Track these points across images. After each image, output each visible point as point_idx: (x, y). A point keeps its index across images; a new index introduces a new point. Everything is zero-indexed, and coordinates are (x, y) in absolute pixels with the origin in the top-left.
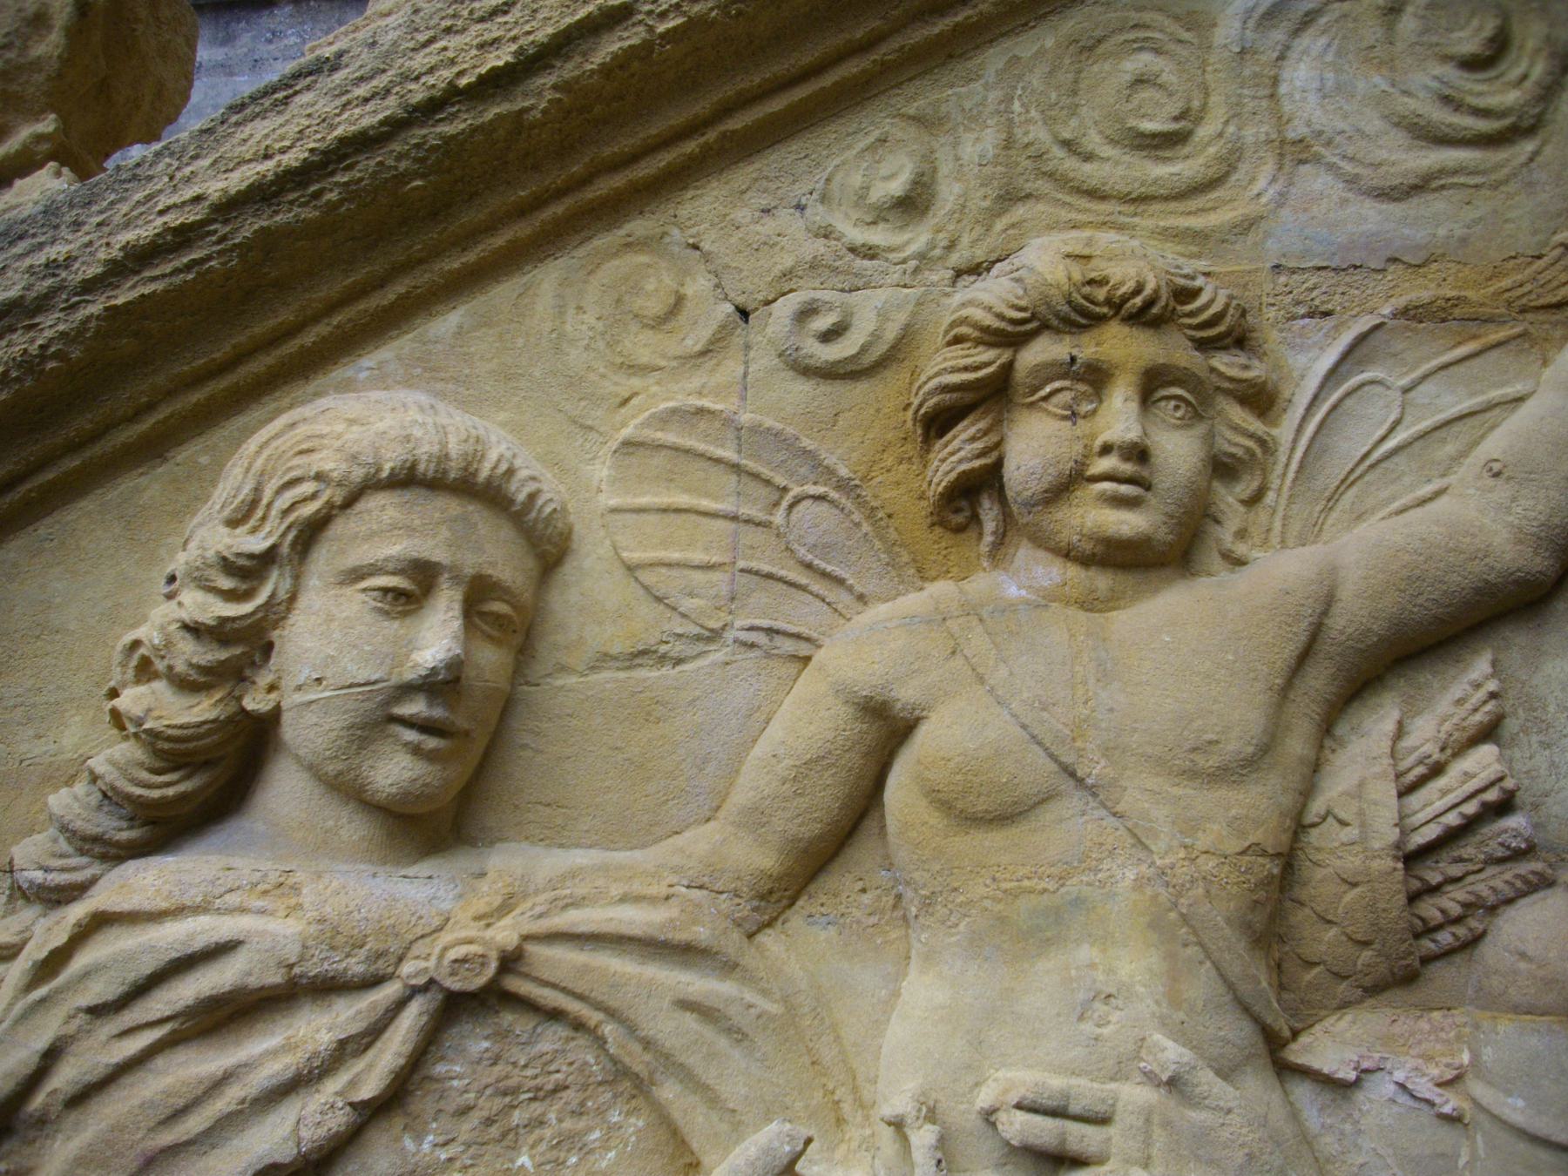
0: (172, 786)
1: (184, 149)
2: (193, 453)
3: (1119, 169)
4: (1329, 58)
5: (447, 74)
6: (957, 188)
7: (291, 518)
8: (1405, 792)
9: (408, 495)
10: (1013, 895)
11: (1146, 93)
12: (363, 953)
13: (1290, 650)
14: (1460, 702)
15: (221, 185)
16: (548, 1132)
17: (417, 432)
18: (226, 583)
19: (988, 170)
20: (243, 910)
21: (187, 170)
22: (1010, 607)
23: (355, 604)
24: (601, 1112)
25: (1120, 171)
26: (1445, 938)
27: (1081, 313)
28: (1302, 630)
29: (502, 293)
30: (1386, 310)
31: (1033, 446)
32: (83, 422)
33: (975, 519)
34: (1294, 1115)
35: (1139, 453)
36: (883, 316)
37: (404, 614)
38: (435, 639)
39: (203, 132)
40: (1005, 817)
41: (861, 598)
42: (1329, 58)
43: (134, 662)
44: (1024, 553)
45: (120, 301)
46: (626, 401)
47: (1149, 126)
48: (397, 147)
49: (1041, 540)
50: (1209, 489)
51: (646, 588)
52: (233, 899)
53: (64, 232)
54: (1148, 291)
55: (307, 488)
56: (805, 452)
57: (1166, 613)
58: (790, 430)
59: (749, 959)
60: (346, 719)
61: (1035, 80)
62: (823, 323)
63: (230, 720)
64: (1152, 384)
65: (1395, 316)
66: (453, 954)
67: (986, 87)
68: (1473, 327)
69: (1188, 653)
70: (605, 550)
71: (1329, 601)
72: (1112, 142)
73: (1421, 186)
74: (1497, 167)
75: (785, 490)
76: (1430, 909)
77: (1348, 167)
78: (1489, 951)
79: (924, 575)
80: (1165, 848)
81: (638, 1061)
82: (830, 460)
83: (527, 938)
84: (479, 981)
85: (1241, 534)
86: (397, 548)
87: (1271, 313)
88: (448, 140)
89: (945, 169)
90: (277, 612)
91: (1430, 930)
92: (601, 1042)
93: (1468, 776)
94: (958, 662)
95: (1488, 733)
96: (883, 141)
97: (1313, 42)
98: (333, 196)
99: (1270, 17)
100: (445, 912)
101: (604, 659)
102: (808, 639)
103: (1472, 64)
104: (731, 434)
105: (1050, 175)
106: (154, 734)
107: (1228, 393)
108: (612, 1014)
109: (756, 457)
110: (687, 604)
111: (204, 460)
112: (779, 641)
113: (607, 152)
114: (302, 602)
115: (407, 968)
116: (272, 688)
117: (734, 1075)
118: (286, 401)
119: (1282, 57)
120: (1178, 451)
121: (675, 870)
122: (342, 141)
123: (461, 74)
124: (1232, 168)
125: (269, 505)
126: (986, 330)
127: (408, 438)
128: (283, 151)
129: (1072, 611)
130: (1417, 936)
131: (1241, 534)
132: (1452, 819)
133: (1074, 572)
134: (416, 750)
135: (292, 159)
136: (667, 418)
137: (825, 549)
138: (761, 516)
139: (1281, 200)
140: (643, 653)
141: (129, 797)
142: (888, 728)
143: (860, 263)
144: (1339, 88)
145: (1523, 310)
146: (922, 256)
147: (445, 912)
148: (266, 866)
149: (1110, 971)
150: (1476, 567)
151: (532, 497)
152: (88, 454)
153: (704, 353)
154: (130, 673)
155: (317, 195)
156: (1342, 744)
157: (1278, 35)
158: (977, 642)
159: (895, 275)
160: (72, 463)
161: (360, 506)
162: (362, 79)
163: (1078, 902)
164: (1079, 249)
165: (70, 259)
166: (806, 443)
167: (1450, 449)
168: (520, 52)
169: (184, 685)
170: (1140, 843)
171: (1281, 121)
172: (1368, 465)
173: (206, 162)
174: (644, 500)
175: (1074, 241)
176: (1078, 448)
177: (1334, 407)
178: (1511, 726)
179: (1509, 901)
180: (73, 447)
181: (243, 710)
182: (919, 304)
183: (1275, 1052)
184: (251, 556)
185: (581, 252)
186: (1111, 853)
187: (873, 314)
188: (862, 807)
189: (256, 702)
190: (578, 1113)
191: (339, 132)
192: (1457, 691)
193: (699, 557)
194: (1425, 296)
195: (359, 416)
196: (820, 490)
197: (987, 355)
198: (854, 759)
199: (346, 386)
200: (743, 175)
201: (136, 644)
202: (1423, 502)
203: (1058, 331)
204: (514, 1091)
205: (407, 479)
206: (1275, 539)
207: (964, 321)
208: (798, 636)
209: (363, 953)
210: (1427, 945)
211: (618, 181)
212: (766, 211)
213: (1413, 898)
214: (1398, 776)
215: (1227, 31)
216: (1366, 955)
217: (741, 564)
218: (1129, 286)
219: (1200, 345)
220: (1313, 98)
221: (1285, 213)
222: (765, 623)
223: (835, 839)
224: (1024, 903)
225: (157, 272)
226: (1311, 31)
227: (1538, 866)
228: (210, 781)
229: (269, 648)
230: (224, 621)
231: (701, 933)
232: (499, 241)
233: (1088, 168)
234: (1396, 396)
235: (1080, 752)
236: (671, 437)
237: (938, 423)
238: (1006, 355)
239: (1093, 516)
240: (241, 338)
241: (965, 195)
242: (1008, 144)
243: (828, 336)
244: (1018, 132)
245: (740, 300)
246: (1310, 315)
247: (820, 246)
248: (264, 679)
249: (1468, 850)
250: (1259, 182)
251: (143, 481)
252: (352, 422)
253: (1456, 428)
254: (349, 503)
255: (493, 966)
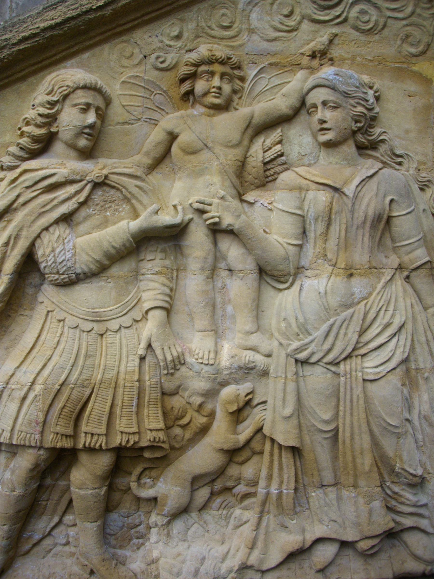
0: (35, 146)
1: (34, 16)
2: (32, 79)
3: (218, 32)
4: (260, 12)
5: (90, 6)
6: (187, 34)
7: (62, 94)
8: (264, 152)
9: (85, 90)
10: (196, 166)
11: (224, 17)
12: (79, 175)
13: (245, 126)
14: (275, 137)
15: (43, 25)
16: (112, 209)
17: (86, 78)
18: (48, 106)
19: (193, 31)
20: (55, 168)
21: (35, 21)
22: (195, 116)
23: (75, 111)
24: (122, 205)
25: (218, 33)
26: (270, 178)
27: (210, 62)
28: (247, 122)
29: (97, 50)
30: (266, 63)
31: (200, 86)
32: (10, 72)
33: (189, 99)
34: (243, 208)
35: (220, 88)
36: (172, 59)
37: (84, 113)
38: (91, 118)
39: (38, 13)
40: (194, 152)
41: (167, 113)
42: (260, 12)
43: (25, 122)
44: (198, 106)
45: (21, 48)
46: (122, 73)
47: (225, 24)
48: (79, 20)
49: (201, 104)
50: (232, 96)
51: (127, 110)
52: (53, 166)
53: (8, 32)
54: (223, 58)
55: (65, 88)
56: (158, 85)
57: (223, 118)
58: (155, 81)
59: (147, 179)
60: (75, 132)
61: (203, 13)
62: (161, 60)
63: (48, 133)
64: (223, 75)
65: (268, 64)
66: (96, 175)
67: (194, 14)
68: (282, 68)
69: (227, 125)
70: (118, 102)
71: (252, 117)
72: (217, 27)
73: (275, 39)
74: (289, 37)
75: (153, 92)
76: (268, 173)
77: (261, 35)
78: (278, 181)
79: (179, 109)
80: (222, 159)
81: (129, 196)
82: (162, 87)
83: (109, 173)
84: (101, 180)
85: (237, 104)
86: (83, 100)
87: (245, 63)
88: (90, 19)
89: (185, 30)
90: (58, 112)
91: (268, 177)
92: (122, 192)
93: (275, 149)
94: (186, 125)
95: (280, 142)
96: (173, 24)
97: (257, 9)
98: (66, 29)
99: (249, 3)
100: (94, 169)
101: (118, 123)
102: (157, 121)
103: (286, 16)
104: (143, 81)
105: (205, 33)
106: (33, 136)
107: (236, 78)
108: (124, 187)
109: (148, 85)
110: (134, 113)
111: (35, 81)
112: (152, 121)
113: (120, 23)
114: (64, 110)
115: (88, 178)
116: (57, 127)
117: (145, 199)
118: (52, 70)
119: (251, 12)
120: (227, 88)
121: (133, 163)
122: (68, 18)
123: (93, 6)
124: (240, 33)
125: (56, 91)
126: (192, 63)
127: (84, 79)
128: (56, 19)
129: (206, 117)
130: (266, 178)
131: (237, 104)
132: (272, 157)
133: (207, 110)
134: (87, 139)
135: (59, 20)
136: (131, 77)
137: (160, 103)
138: (149, 97)
139: (249, 40)
140: (125, 122)
141: (28, 148)
142: (173, 137)
143: (168, 48)
144: (261, 19)
145: (292, 65)
146: (180, 47)
147: (94, 169)
148: (58, 160)
149: (212, 180)
150: (279, 112)
151: (106, 91)
152: (10, 79)
153: (137, 64)
154: (24, 124)
155: (63, 28)
156: (254, 144)
157: (250, 7)
158: (189, 122)
159: (175, 51)
160: (7, 81)
161: (76, 92)
162: (72, 5)
163: (207, 168)
164: (210, 49)
165: (10, 39)
166: (158, 83)
167: (276, 90)
168: (105, 2)
169: (38, 126)
170: (218, 158)
171: (250, 25)
172: (262, 92)
173: (39, 20)
174: (126, 93)
175: (209, 46)
176: (208, 87)
177: (256, 81)
178: (284, 142)
179: (282, 172)
180: (7, 77)
181: (51, 131)
182: (179, 57)
183: (240, 196)
184: (54, 101)
185: (113, 42)
186: (213, 160)
187: (171, 58)
188: (167, 152)
189: (53, 130)
190: (117, 205)
191: (68, 16)
192: (274, 135)
193: (137, 104)
194: (274, 61)
195: (71, 74)
196: (160, 92)
197: (193, 68)
198: (166, 143)
199: (65, 68)
200: (145, 29)
201: (26, 118)
202: (271, 100)
203: (206, 64)
204: (106, 201)
205: (85, 87)
206: (243, 105)
207: (188, 61)
208: (155, 120)
209: (79, 175)
210: (267, 180)
211: (121, 29)
212: (150, 36)
213: (265, 171)
214: (263, 149)
215: (241, 6)
216: (256, 180)
217: (145, 106)
218: (219, 57)
219: (232, 69)
220: (256, 21)
221: (249, 43)
222: (149, 117)
223: (162, 158)
224: (197, 168)
225: (29, 42)
226: (257, 6)
227: (287, 166)
228: (43, 146)
229: (56, 119)
230: (49, 113)
231: (138, 174)
232: (97, 39)
233: (212, 32)
234: (267, 80)
235: (207, 142)
236: (131, 81)
237: (182, 81)
238: (196, 69)
239: (211, 100)
240: (44, 56)
241: (189, 36)
242: (197, 26)
243: (162, 62)
244: (199, 24)
245: (145, 54)
246: (253, 63)
247: (160, 45)
248: (55, 125)
249: (275, 163)
250: (245, 37)
251: (21, 85)
252: (72, 75)
253: (278, 87)
254: (74, 91)
255: (104, 178)
